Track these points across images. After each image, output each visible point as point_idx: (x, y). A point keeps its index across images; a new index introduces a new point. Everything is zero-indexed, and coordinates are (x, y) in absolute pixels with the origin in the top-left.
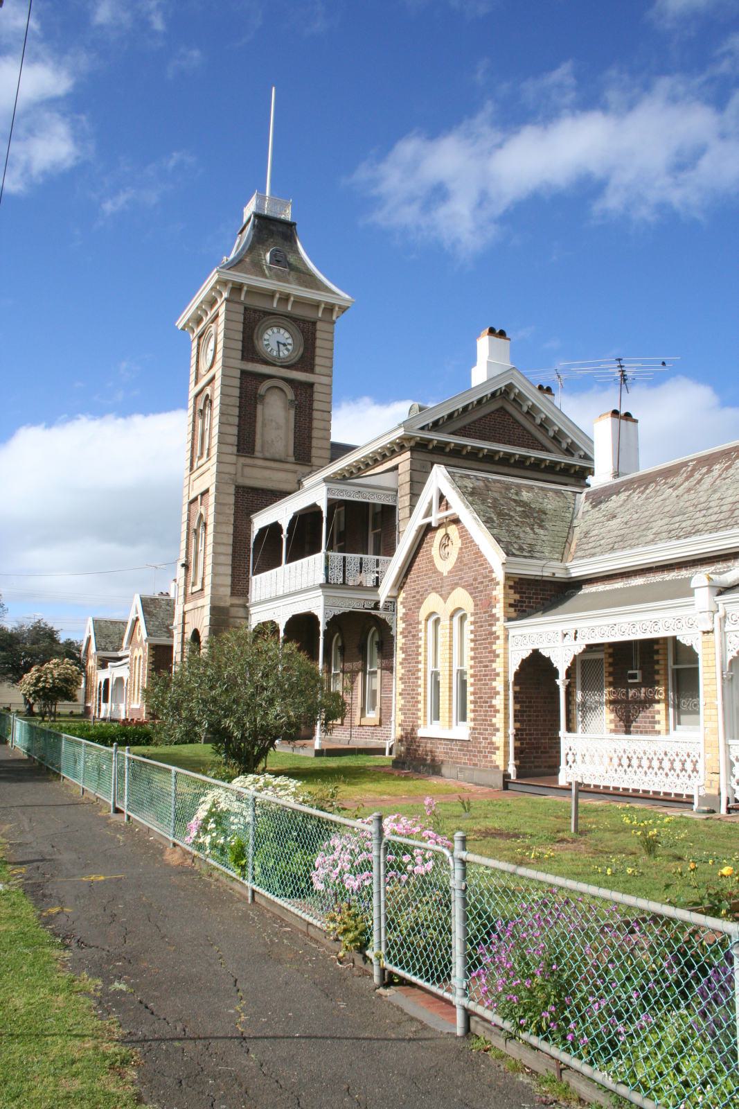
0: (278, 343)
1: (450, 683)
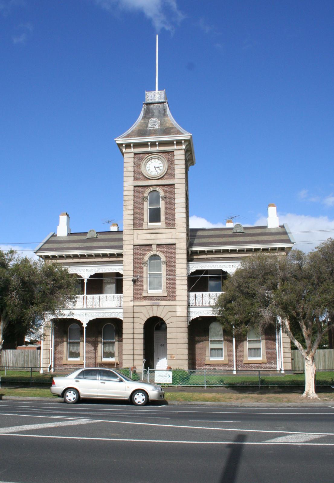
0: (155, 167)
1: (293, 443)
